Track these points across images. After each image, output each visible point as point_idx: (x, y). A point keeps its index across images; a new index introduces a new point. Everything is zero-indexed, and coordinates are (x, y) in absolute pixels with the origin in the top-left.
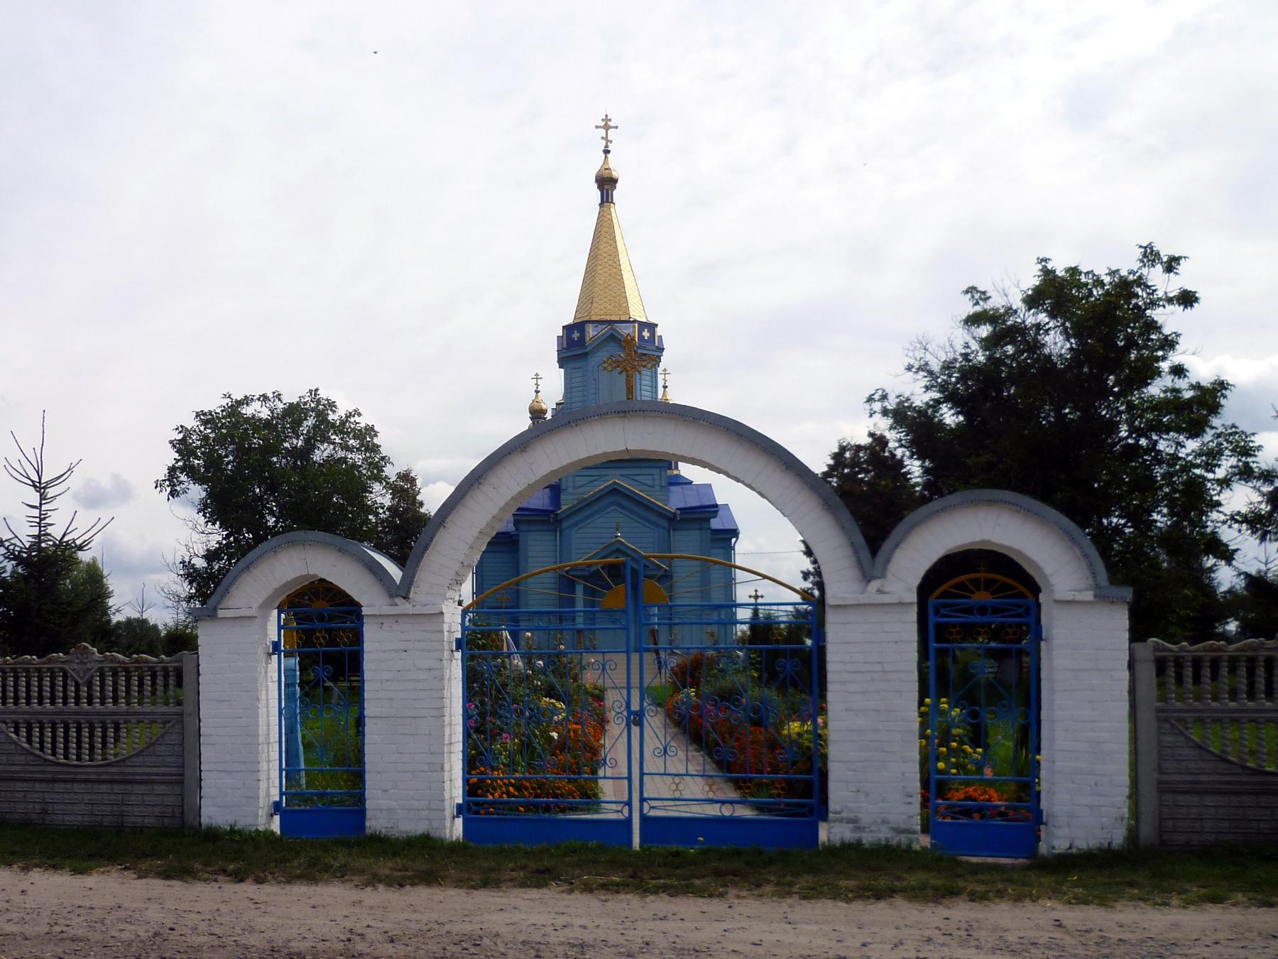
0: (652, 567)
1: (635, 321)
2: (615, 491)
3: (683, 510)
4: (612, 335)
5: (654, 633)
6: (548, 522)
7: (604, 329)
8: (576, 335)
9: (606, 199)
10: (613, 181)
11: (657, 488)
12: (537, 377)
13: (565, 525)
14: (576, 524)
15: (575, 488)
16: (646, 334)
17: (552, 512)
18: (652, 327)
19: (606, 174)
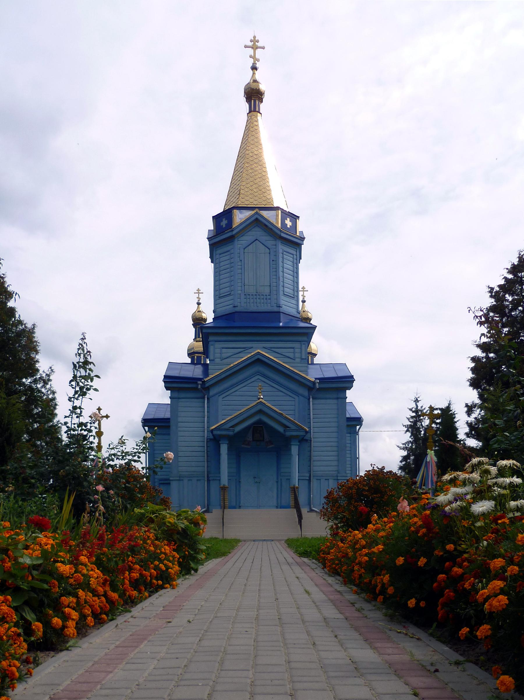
0: (293, 427)
1: (278, 208)
2: (258, 361)
3: (323, 380)
4: (257, 219)
5: (294, 490)
6: (196, 389)
7: (247, 214)
8: (224, 223)
9: (253, 110)
11: (298, 360)
13: (212, 392)
16: (288, 223)
17: (200, 379)
18: (295, 218)
19: (254, 86)
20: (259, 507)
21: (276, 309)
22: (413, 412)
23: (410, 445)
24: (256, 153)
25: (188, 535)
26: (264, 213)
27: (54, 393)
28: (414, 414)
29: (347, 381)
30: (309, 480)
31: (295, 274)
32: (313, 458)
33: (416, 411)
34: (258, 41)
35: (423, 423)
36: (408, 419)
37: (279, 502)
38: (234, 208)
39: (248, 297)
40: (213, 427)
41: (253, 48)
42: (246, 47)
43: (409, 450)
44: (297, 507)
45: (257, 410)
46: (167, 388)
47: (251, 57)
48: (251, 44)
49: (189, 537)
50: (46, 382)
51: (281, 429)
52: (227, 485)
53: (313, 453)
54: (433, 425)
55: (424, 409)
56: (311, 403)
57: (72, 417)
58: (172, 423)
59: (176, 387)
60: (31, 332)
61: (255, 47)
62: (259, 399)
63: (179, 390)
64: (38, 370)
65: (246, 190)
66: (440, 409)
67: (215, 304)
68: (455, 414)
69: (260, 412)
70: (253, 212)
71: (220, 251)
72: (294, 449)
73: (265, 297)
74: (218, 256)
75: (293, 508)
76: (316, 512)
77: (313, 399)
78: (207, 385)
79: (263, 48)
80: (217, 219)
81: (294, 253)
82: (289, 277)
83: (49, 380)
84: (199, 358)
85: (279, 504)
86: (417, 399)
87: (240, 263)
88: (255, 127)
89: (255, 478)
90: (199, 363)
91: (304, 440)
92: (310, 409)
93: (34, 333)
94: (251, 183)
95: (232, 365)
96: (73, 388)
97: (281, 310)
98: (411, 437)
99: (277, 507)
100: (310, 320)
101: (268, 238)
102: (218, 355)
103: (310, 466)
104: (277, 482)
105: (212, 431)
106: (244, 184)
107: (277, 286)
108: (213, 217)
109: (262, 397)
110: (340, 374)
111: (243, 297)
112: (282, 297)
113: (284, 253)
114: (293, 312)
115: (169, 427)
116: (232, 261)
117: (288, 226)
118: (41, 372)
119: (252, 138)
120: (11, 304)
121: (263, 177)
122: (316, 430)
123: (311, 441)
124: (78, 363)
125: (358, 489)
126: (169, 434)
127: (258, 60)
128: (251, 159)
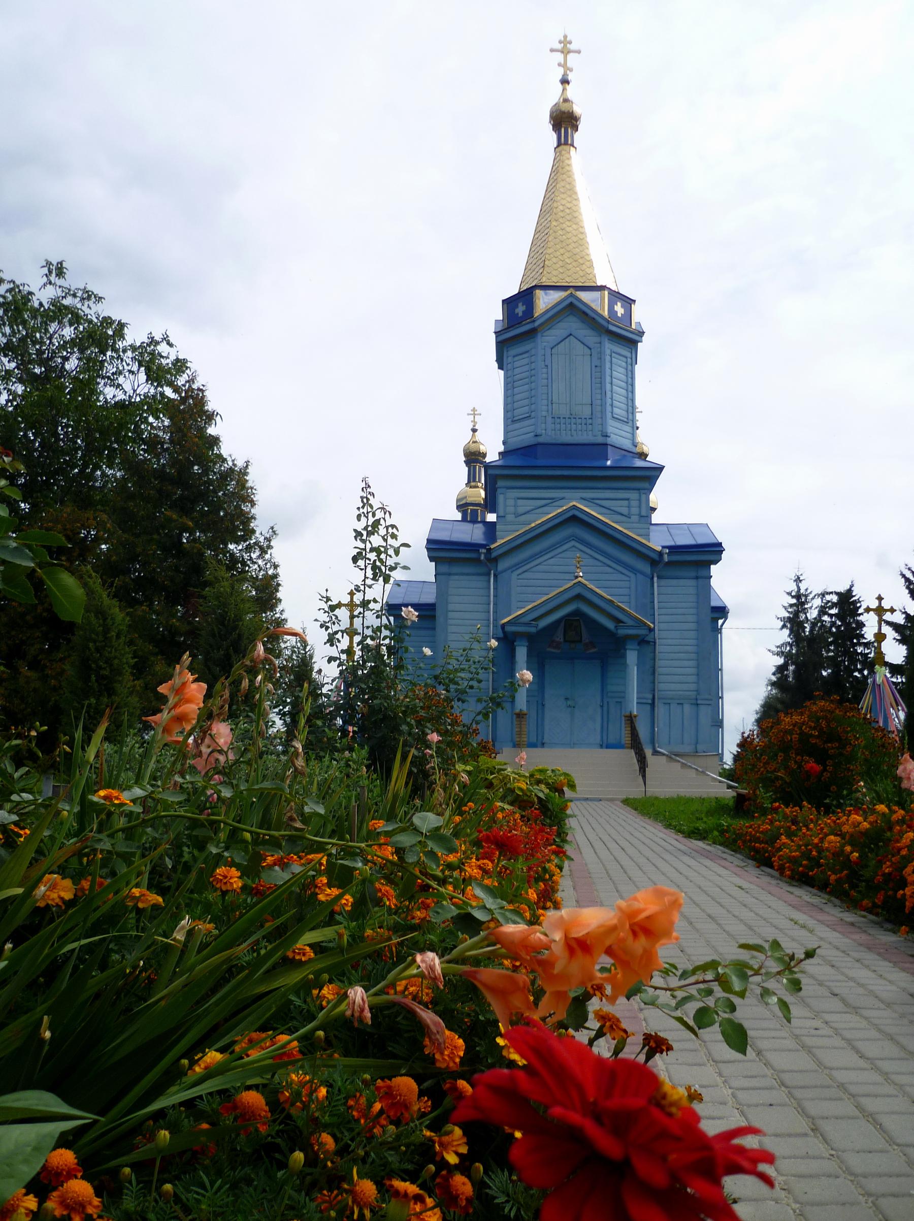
0: (630, 622)
1: (602, 288)
2: (574, 519)
3: (675, 549)
4: (571, 304)
6: (477, 561)
7: (555, 296)
8: (520, 309)
9: (564, 142)
10: (568, 82)
11: (635, 518)
12: (474, 412)
13: (502, 565)
14: (517, 566)
15: (517, 515)
16: (619, 309)
18: (629, 302)
19: (565, 107)
20: (572, 745)
21: (600, 440)
22: (793, 597)
23: (788, 648)
24: (568, 205)
25: (549, 809)
26: (584, 296)
27: (276, 567)
28: (794, 601)
29: (711, 552)
30: (653, 705)
31: (630, 387)
32: (659, 670)
33: (798, 596)
34: (570, 43)
35: (808, 615)
36: (785, 608)
37: (605, 738)
38: (536, 287)
39: (558, 420)
40: (505, 620)
41: (562, 52)
42: (552, 50)
43: (788, 656)
44: (636, 745)
45: (574, 594)
46: (431, 559)
47: (559, 65)
48: (560, 46)
49: (549, 813)
50: (263, 551)
51: (610, 625)
52: (524, 709)
53: (659, 663)
54: (826, 618)
55: (811, 593)
56: (655, 585)
57: (363, 617)
58: (439, 613)
59: (445, 558)
60: (244, 472)
61: (566, 52)
62: (577, 577)
63: (451, 561)
64: (253, 531)
65: (554, 260)
66: (837, 593)
67: (506, 432)
68: (860, 602)
69: (579, 597)
70: (569, 292)
71: (513, 351)
72: (632, 657)
73: (584, 421)
74: (510, 359)
75: (627, 748)
76: (664, 754)
77: (658, 577)
78: (494, 555)
79: (579, 52)
80: (509, 303)
81: (629, 355)
82: (619, 392)
83: (270, 547)
84: (474, 513)
85: (605, 741)
86: (799, 578)
87: (545, 370)
88: (567, 168)
89: (567, 699)
90: (474, 521)
91: (646, 642)
92: (653, 594)
93: (246, 474)
94: (562, 251)
95: (533, 525)
96: (362, 569)
97: (609, 441)
98: (789, 636)
99: (601, 746)
100: (646, 455)
101: (588, 332)
102: (512, 509)
103: (654, 683)
104: (602, 706)
105: (503, 626)
106: (549, 251)
107: (603, 405)
108: (504, 301)
109: (581, 574)
110: (701, 540)
111: (549, 419)
112: (611, 422)
113: (613, 355)
114: (626, 444)
115: (433, 617)
116: (533, 366)
117: (619, 315)
118: (257, 534)
119: (562, 184)
120: (211, 431)
121: (581, 242)
122: (663, 626)
123: (655, 643)
124: (365, 528)
125: (802, 733)
126: (434, 629)
127: (571, 70)
128: (562, 214)
